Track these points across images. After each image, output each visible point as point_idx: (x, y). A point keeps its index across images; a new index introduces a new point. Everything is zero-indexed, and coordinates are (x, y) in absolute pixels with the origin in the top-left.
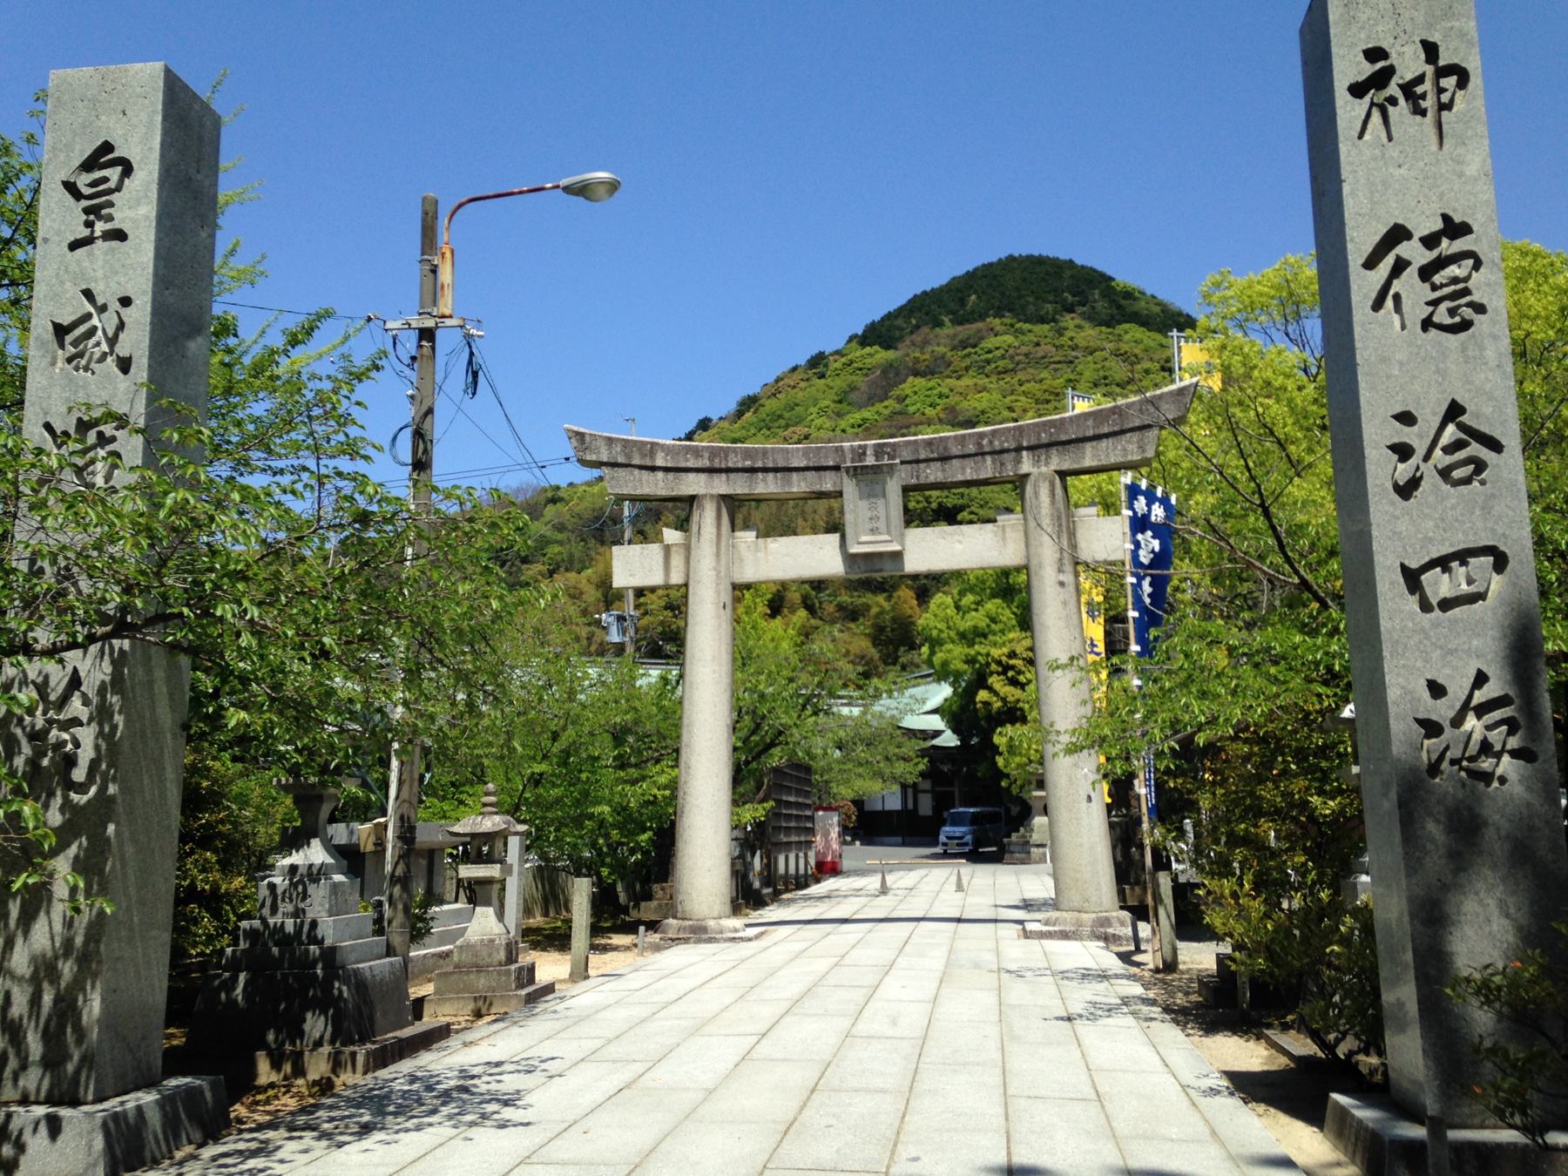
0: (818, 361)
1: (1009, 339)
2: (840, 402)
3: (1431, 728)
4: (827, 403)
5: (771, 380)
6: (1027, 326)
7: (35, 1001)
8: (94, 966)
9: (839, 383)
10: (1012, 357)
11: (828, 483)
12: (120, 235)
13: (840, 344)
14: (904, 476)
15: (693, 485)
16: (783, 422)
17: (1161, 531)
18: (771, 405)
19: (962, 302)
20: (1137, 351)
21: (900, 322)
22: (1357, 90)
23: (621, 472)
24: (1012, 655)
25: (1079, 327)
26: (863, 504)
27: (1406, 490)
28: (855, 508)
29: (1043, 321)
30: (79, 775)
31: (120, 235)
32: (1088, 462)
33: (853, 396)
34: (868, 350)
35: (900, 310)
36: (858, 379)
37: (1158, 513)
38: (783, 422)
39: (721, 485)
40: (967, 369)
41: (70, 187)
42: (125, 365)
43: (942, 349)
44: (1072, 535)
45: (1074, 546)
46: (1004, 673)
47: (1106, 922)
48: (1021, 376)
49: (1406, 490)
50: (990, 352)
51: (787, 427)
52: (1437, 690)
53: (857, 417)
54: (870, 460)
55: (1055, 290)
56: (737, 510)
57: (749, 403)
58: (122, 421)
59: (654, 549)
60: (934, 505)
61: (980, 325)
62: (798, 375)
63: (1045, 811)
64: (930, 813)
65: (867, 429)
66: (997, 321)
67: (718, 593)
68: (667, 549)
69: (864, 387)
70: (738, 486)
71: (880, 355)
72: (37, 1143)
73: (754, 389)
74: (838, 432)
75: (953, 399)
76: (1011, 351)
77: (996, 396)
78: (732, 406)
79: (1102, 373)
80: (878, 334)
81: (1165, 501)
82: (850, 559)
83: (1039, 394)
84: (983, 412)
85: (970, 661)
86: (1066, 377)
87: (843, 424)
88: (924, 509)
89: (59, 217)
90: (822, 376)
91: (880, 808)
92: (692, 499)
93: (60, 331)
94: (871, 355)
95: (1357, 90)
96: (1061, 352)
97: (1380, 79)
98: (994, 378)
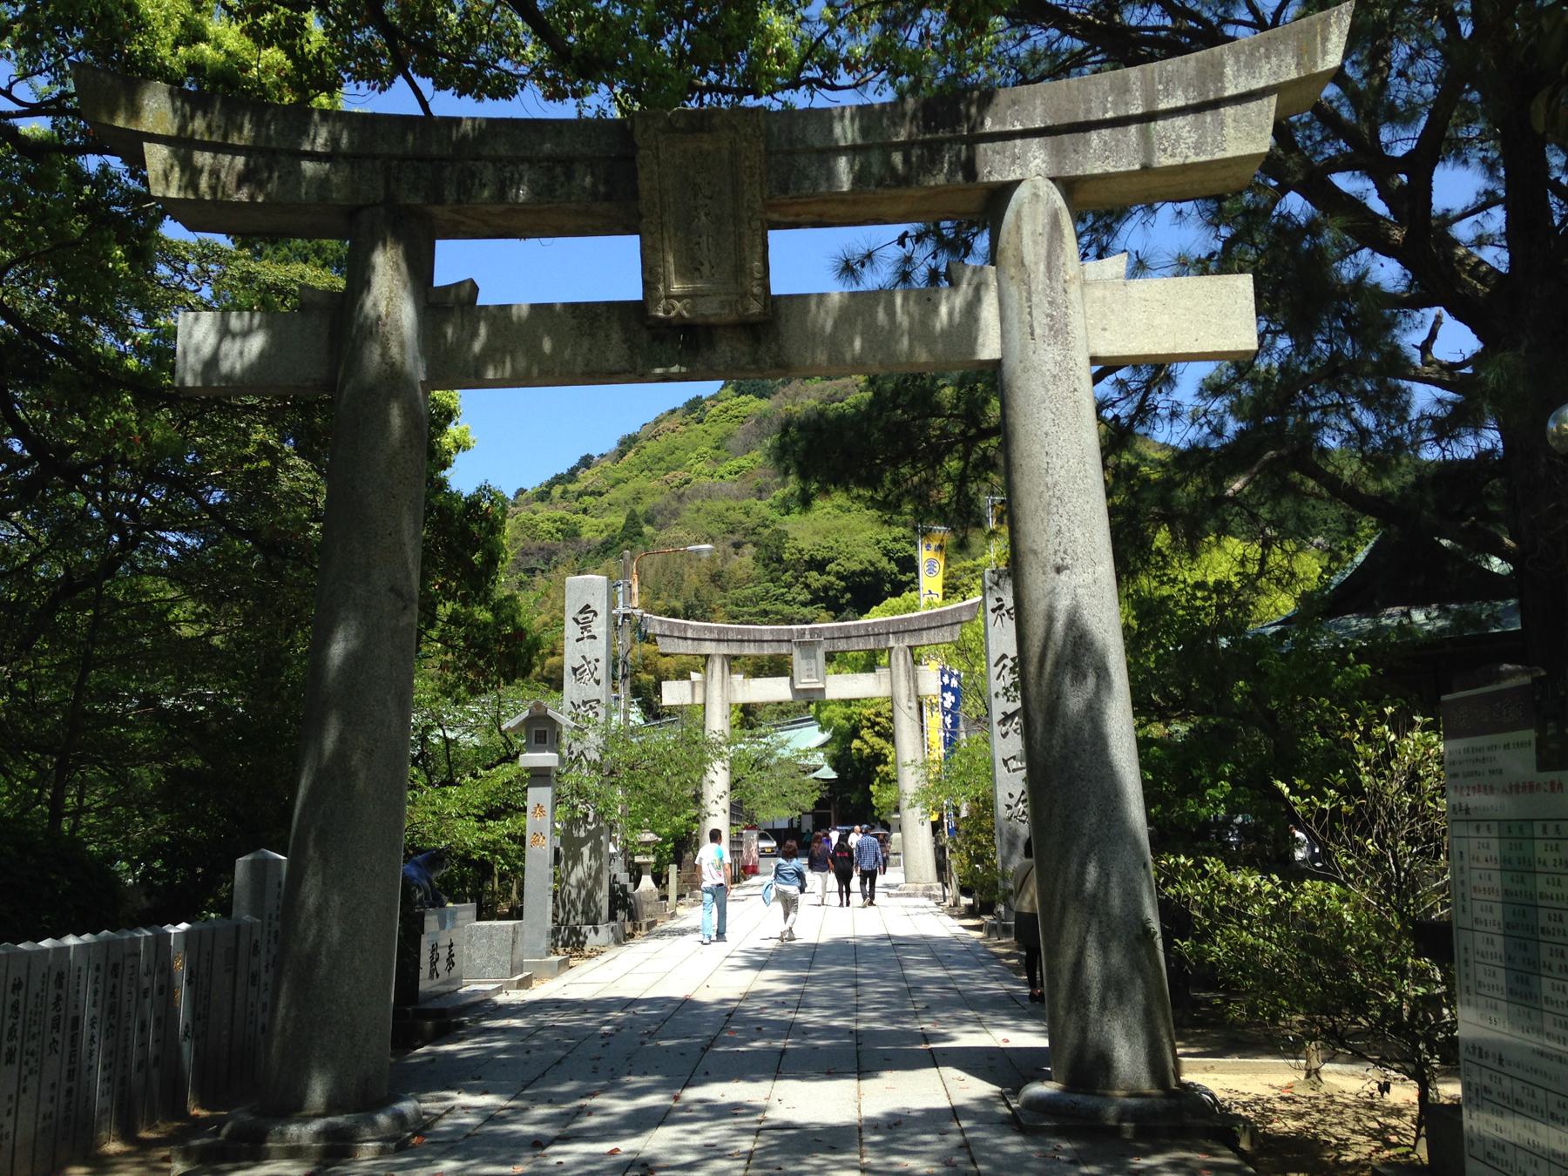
2: (718, 448)
3: (1009, 807)
5: (650, 419)
7: (579, 893)
9: (717, 430)
11: (784, 649)
12: (594, 637)
14: (826, 646)
15: (709, 648)
16: (664, 465)
17: (955, 692)
18: (652, 447)
22: (993, 611)
23: (668, 640)
24: (878, 714)
26: (804, 662)
27: (1004, 736)
28: (798, 662)
30: (590, 819)
31: (594, 637)
32: (925, 641)
33: (730, 443)
34: (743, 398)
36: (733, 426)
37: (954, 683)
38: (664, 465)
39: (724, 649)
41: (576, 620)
42: (598, 682)
44: (916, 681)
45: (916, 687)
46: (872, 727)
47: (931, 888)
49: (1004, 736)
51: (668, 470)
52: (1011, 796)
53: (734, 464)
54: (807, 638)
56: (732, 662)
57: (628, 443)
58: (598, 701)
59: (686, 682)
60: (806, 557)
61: (846, 380)
62: (677, 418)
63: (900, 829)
65: (744, 476)
68: (693, 684)
69: (738, 434)
70: (734, 650)
72: (591, 935)
73: (633, 428)
74: (716, 479)
78: (611, 445)
81: (958, 676)
82: (796, 692)
85: (848, 719)
87: (721, 471)
89: (571, 630)
90: (700, 421)
92: (707, 656)
93: (575, 670)
94: (746, 404)
95: (993, 611)
97: (1000, 607)
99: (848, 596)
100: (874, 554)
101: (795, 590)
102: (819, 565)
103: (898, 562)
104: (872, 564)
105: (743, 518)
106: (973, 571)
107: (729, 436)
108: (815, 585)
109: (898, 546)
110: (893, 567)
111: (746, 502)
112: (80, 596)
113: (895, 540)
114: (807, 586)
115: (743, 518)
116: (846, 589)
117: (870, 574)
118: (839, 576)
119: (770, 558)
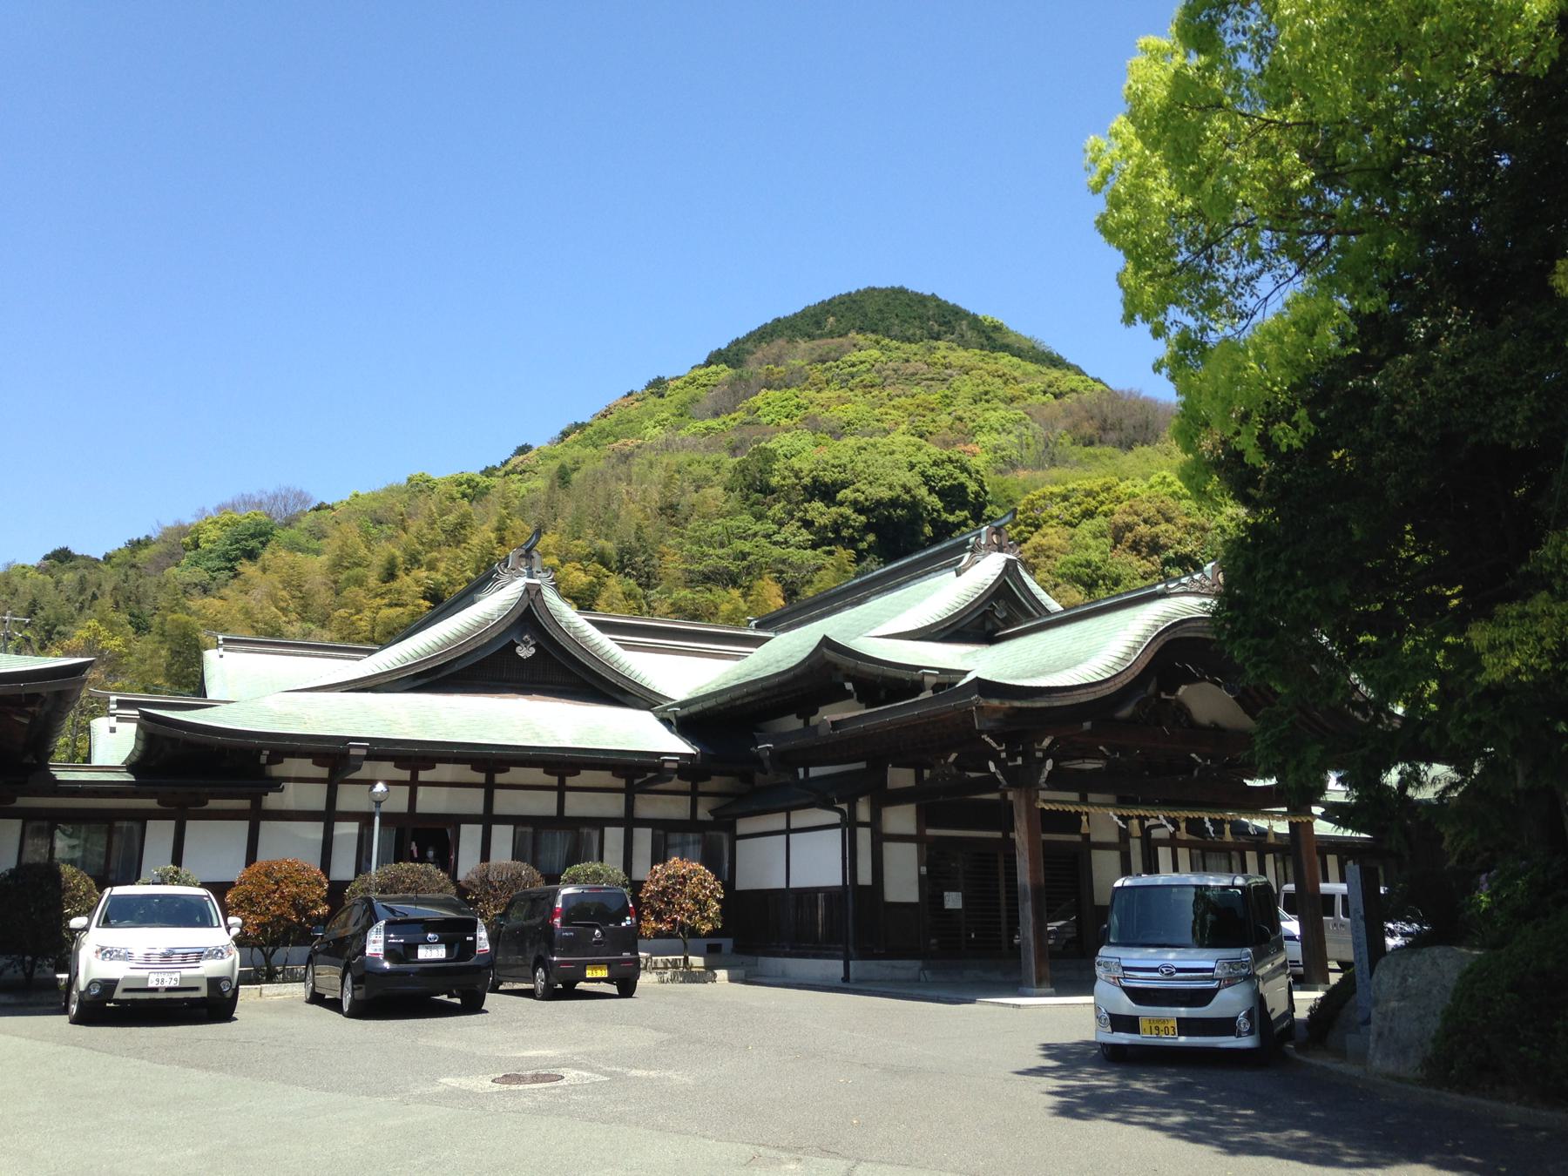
0: (658, 386)
1: (875, 353)
4: (665, 415)
6: (895, 343)
8: (1240, 563)
10: (879, 372)
13: (683, 369)
19: (818, 324)
20: (1016, 374)
21: (749, 346)
25: (950, 348)
29: (909, 340)
35: (750, 335)
40: (828, 382)
43: (798, 362)
48: (889, 390)
50: (853, 365)
55: (920, 317)
60: (807, 481)
64: (912, 896)
66: (860, 337)
67: (743, 697)
71: (724, 372)
75: (813, 410)
76: (877, 365)
77: (863, 408)
79: (981, 389)
80: (731, 356)
83: (912, 409)
84: (848, 424)
86: (940, 392)
88: (793, 487)
91: (780, 884)
96: (934, 370)
98: (859, 392)
99: (871, 538)
100: (912, 479)
101: (787, 531)
102: (825, 491)
103: (942, 494)
104: (908, 491)
105: (710, 473)
106: (1065, 498)
107: (694, 400)
108: (821, 521)
109: (943, 473)
110: (934, 501)
111: (714, 457)
112: (1244, 971)
113: (935, 464)
114: (807, 524)
115: (710, 473)
116: (868, 528)
117: (904, 506)
118: (859, 508)
119: (749, 487)
